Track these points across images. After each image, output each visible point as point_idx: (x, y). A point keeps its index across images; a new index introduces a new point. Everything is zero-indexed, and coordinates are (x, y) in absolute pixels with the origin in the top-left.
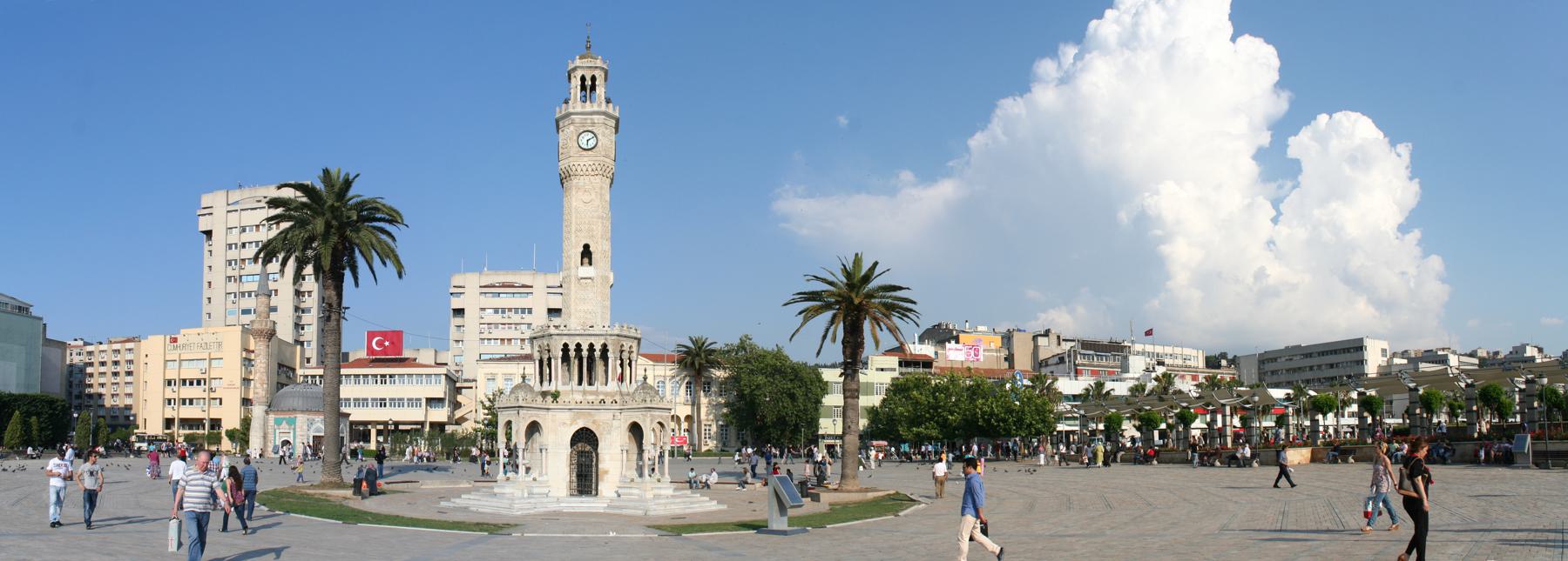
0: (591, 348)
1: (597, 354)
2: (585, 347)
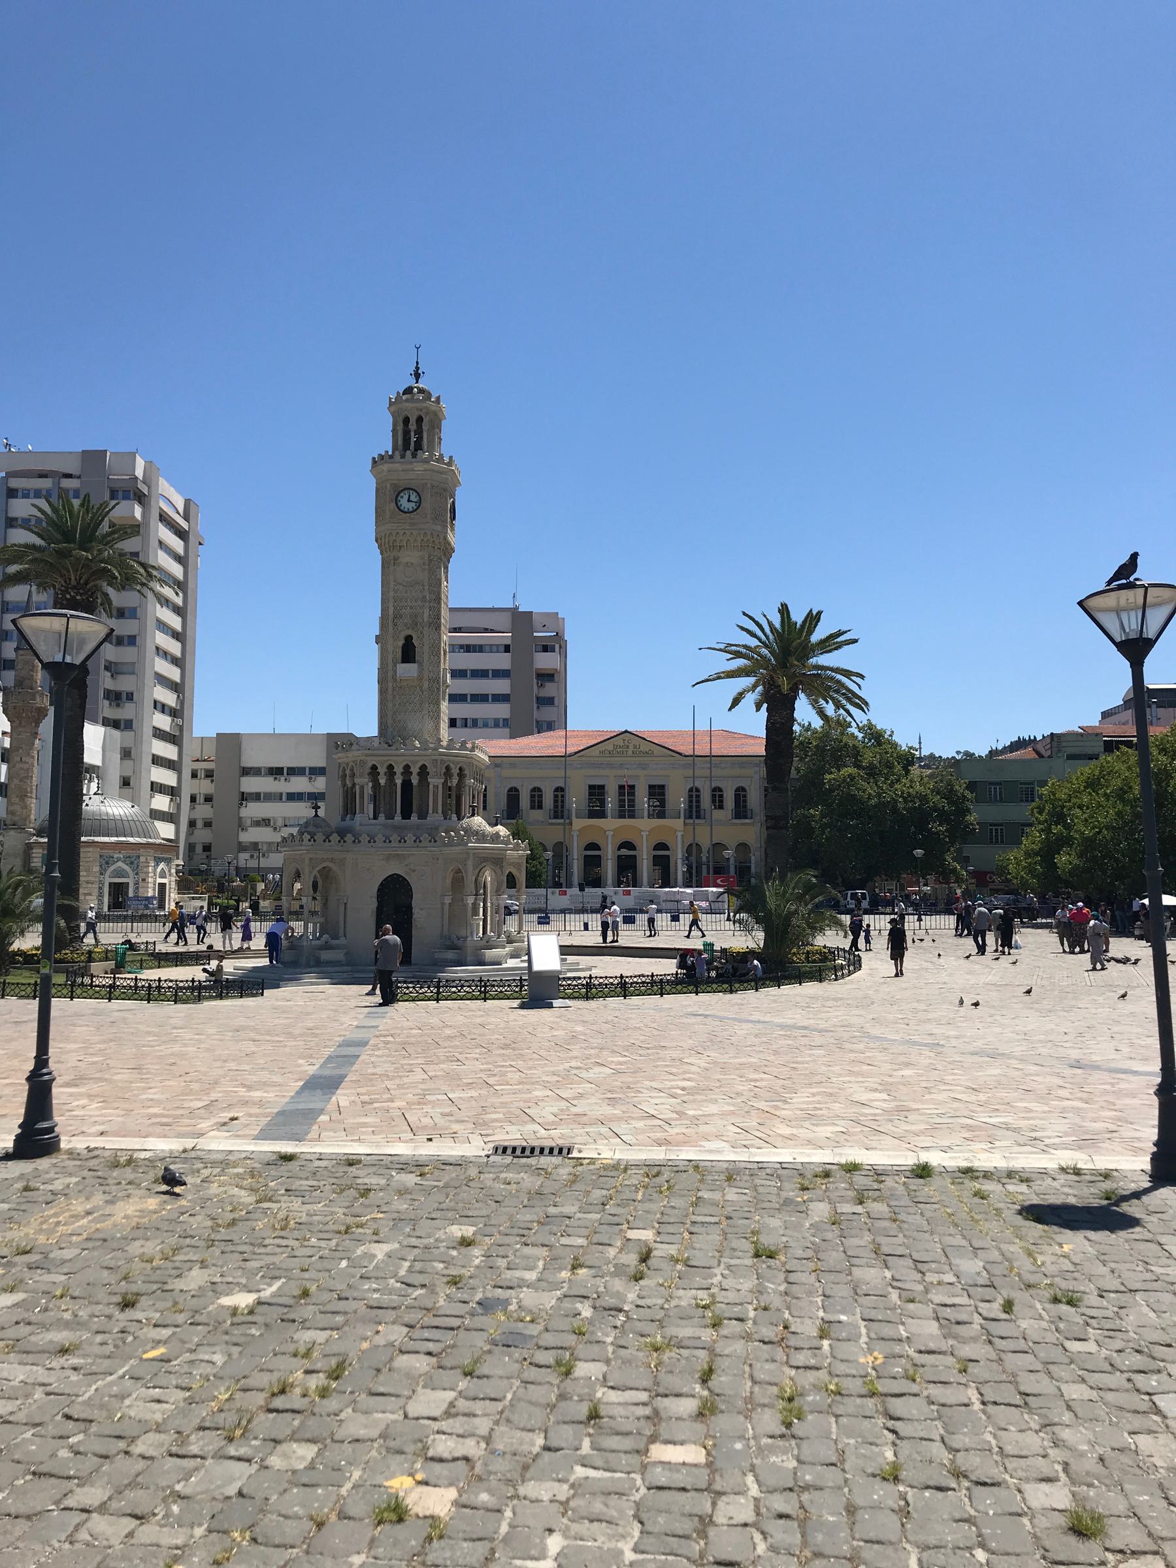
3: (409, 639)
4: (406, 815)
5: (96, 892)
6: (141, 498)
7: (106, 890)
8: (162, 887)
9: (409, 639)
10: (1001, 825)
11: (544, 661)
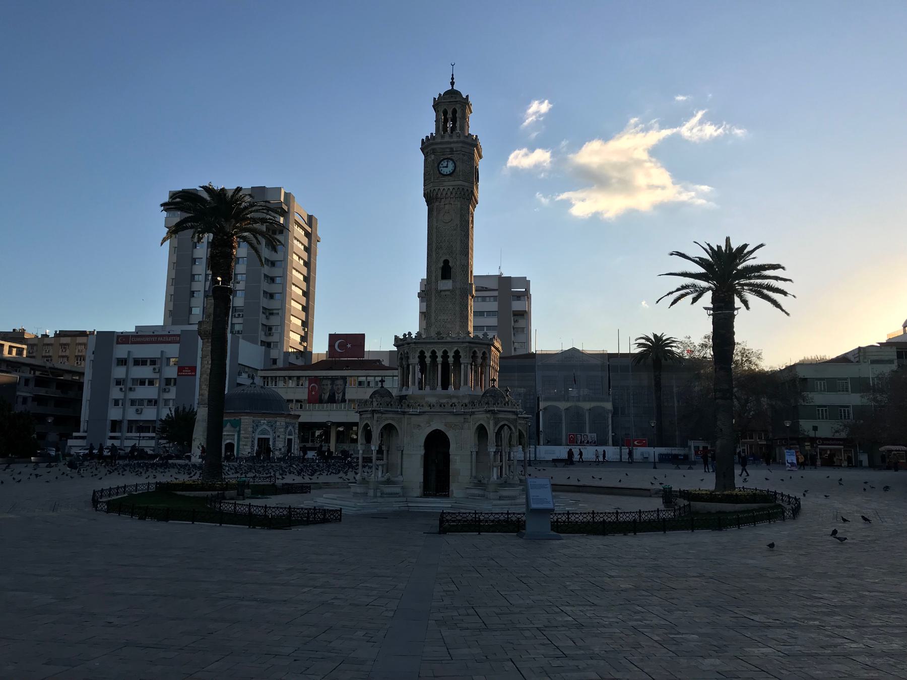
0: (445, 355)
1: (451, 360)
2: (439, 354)
3: (446, 262)
4: (445, 386)
5: (249, 444)
6: (284, 213)
7: (256, 442)
8: (290, 441)
9: (446, 262)
10: (825, 406)
11: (517, 306)
